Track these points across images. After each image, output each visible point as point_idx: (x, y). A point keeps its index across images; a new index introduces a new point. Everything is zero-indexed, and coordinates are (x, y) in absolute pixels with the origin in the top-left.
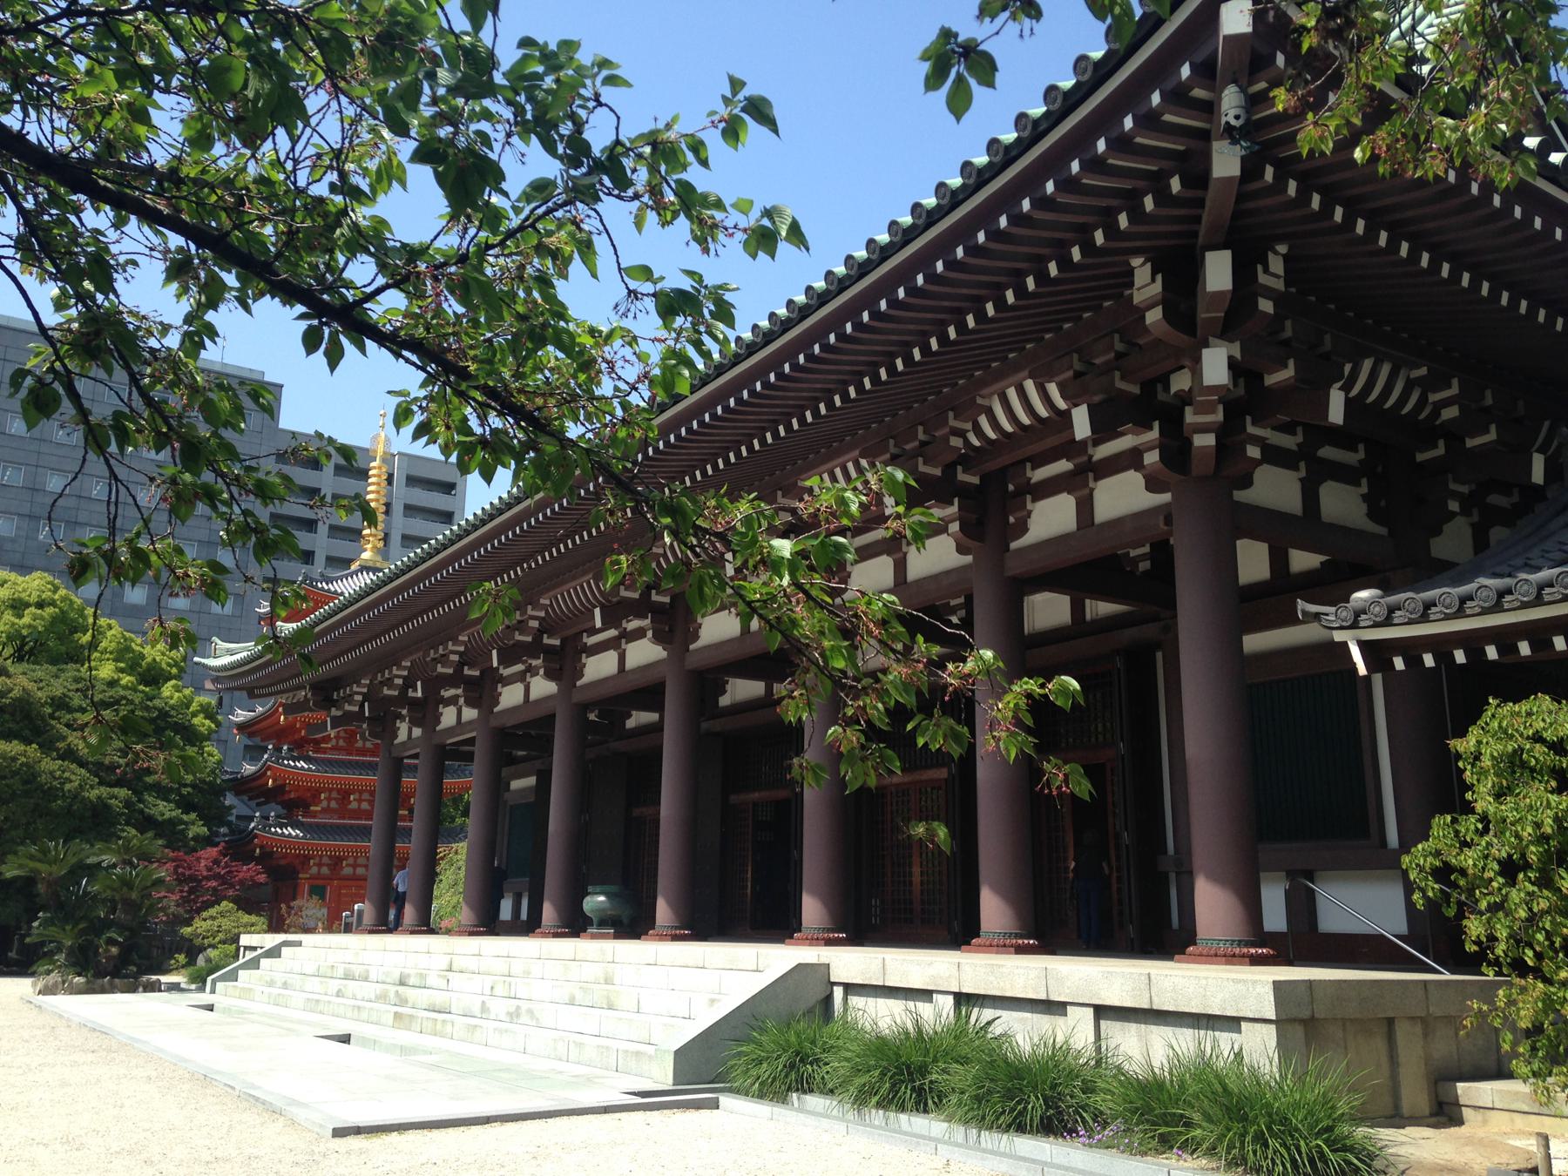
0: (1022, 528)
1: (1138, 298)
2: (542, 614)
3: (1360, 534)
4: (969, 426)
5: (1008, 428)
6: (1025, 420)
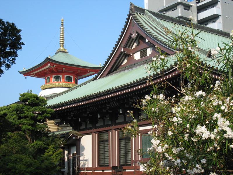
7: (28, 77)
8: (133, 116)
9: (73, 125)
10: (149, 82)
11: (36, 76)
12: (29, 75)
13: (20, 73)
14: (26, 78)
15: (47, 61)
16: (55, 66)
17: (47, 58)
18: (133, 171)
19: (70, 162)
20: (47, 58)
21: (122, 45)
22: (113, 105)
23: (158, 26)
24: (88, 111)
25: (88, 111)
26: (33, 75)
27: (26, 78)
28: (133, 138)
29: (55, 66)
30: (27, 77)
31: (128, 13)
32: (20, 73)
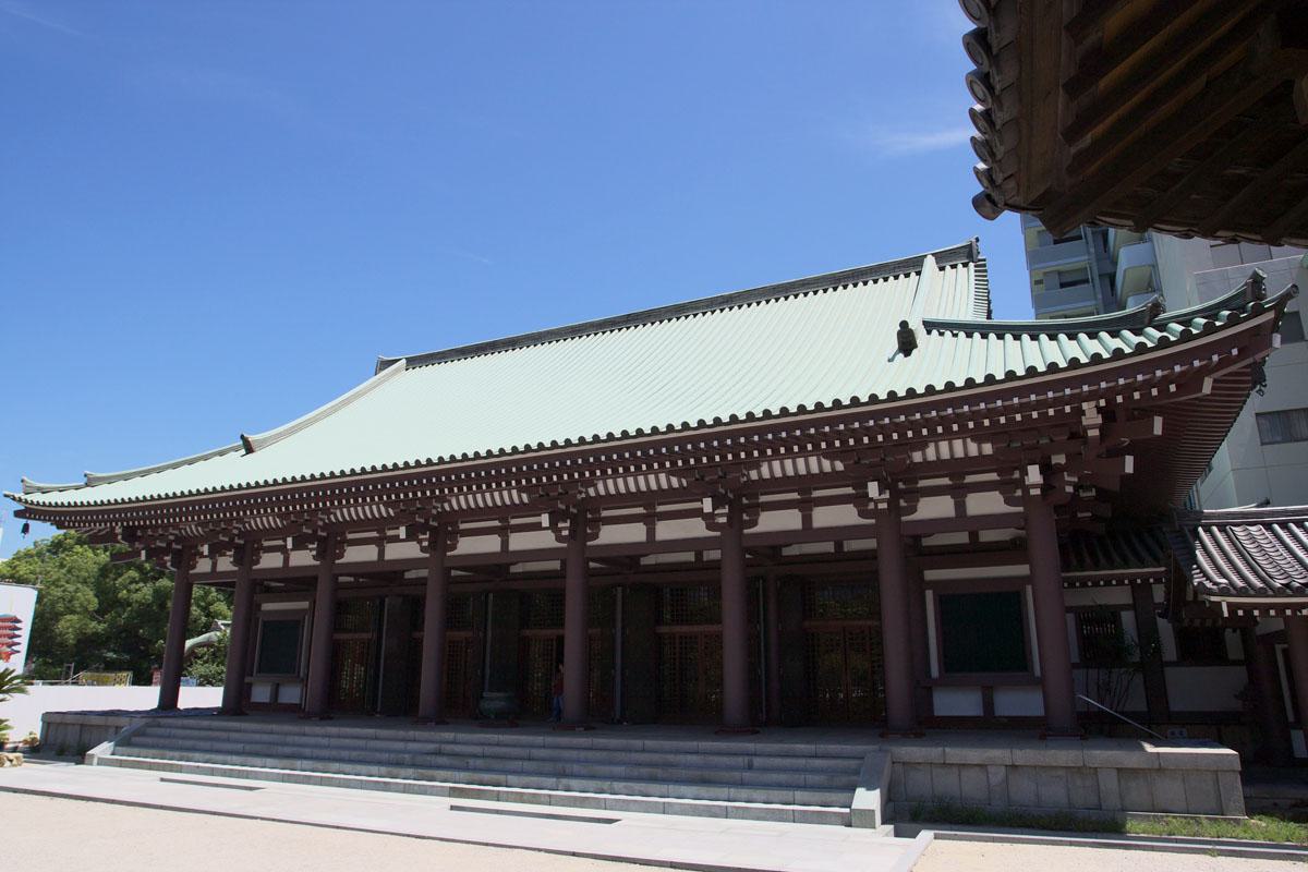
0: (454, 547)
1: (1085, 421)
2: (176, 532)
4: (439, 505)
5: (355, 518)
6: (341, 519)
22: (186, 532)
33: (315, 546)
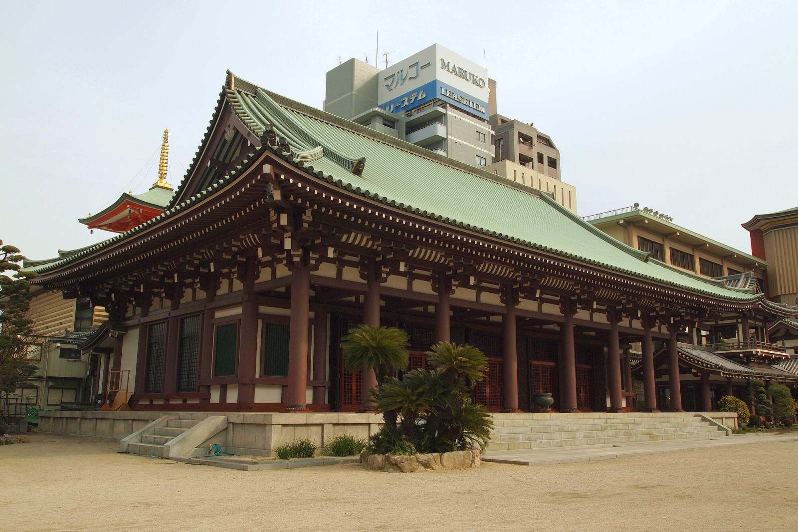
3: (559, 316)
7: (94, 230)
8: (15, 263)
9: (110, 309)
10: (755, 406)
11: (111, 230)
12: (99, 227)
13: (81, 221)
14: (92, 231)
15: (125, 201)
16: (141, 211)
17: (124, 194)
18: (198, 402)
19: (761, 334)
20: (124, 194)
21: (210, 154)
23: (267, 109)
24: (131, 280)
25: (131, 280)
26: (105, 228)
27: (92, 231)
28: (40, 331)
29: (141, 211)
30: (93, 229)
31: (221, 91)
32: (81, 221)
33: (198, 280)
